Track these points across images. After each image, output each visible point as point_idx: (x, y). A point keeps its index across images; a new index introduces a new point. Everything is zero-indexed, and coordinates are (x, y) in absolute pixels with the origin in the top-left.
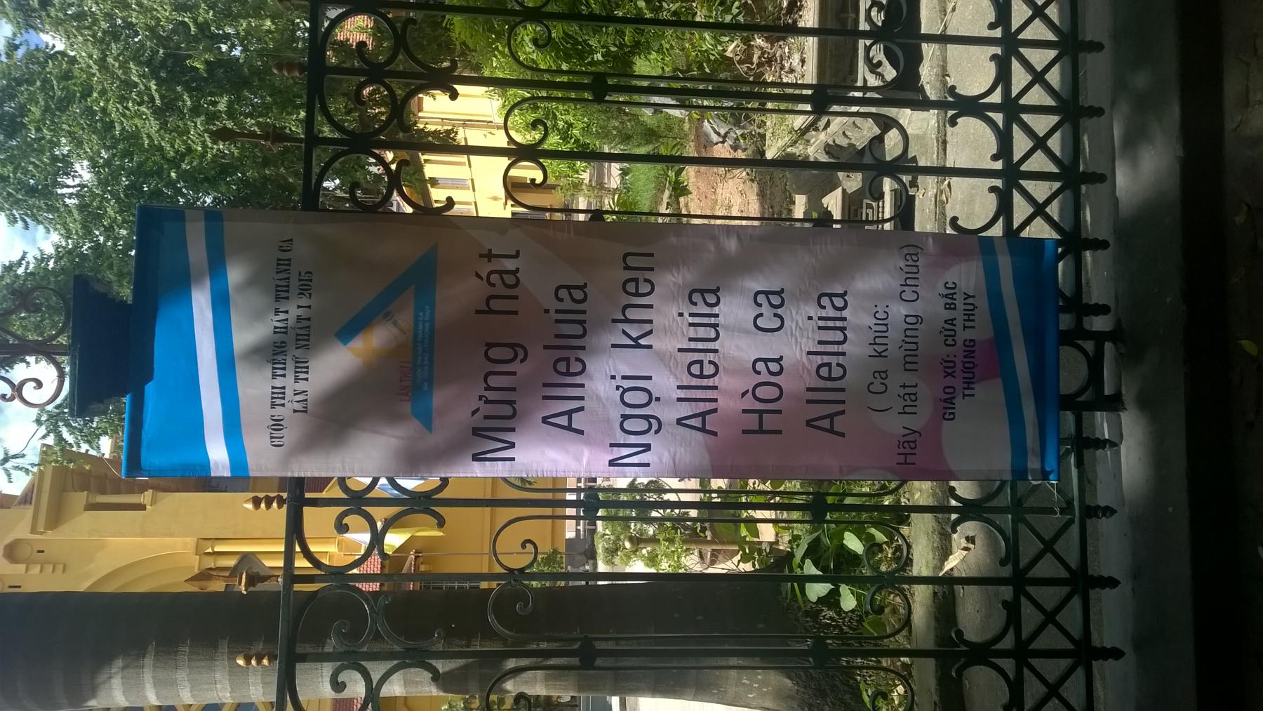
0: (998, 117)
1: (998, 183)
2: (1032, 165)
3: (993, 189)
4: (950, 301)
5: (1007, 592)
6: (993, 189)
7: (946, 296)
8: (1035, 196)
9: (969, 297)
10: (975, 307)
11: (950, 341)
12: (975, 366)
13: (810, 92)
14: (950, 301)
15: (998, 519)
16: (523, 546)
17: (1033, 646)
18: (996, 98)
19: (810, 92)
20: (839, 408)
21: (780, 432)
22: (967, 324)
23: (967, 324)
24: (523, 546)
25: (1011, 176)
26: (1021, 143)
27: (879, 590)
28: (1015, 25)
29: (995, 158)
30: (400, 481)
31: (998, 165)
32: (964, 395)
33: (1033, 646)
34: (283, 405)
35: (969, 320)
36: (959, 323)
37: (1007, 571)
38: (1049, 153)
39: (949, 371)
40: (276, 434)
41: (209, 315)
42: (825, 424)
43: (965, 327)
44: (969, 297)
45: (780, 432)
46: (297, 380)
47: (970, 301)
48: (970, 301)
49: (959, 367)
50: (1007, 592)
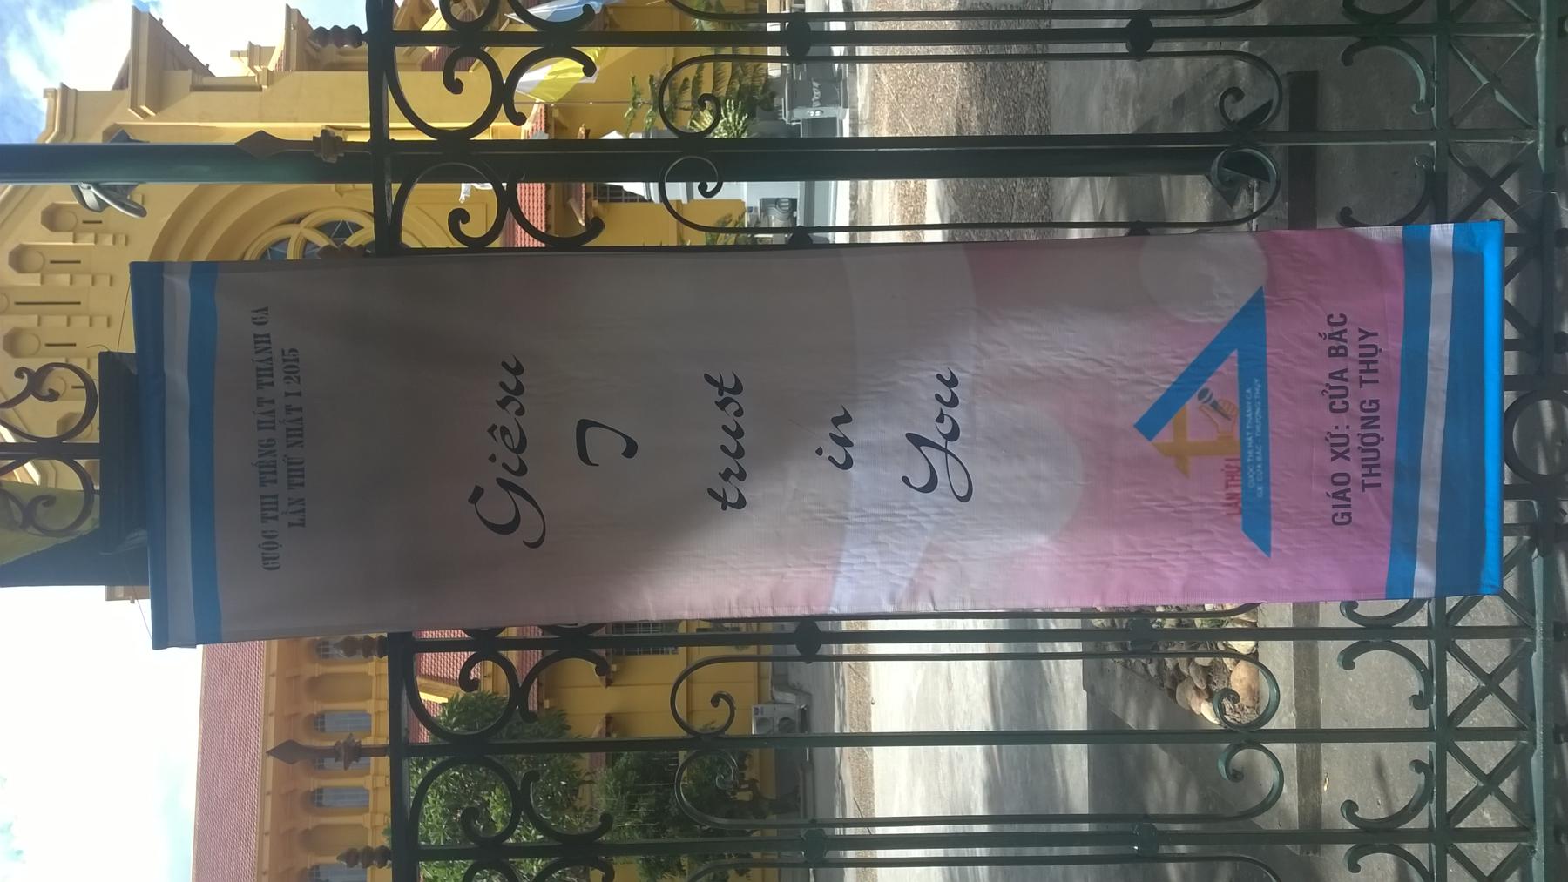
0: (1420, 648)
2: (1476, 719)
4: (1334, 343)
5: (1424, 750)
6: (1418, 765)
7: (1331, 336)
8: (1481, 866)
9: (1368, 334)
10: (1378, 351)
11: (1339, 405)
13: (1124, 23)
14: (1334, 343)
15: (1411, 848)
19: (1124, 23)
22: (1365, 377)
26: (1460, 681)
27: (1238, 747)
28: (1454, 701)
30: (533, 11)
31: (1420, 719)
32: (1364, 486)
34: (275, 518)
35: (1368, 371)
36: (1353, 374)
37: (1420, 719)
38: (1502, 696)
39: (1340, 450)
40: (271, 554)
44: (1368, 334)
46: (291, 486)
47: (1368, 341)
48: (1368, 341)
49: (1355, 443)
50: (1424, 750)
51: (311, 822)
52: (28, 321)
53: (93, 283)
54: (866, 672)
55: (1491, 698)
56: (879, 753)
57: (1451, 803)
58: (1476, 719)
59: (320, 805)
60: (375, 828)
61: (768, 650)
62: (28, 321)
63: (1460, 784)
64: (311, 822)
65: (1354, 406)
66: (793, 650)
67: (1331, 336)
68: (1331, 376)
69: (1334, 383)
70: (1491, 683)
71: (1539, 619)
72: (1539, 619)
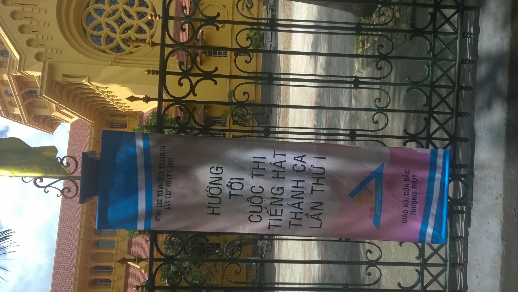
1: (418, 268)
3: (417, 271)
5: (426, 115)
12: (417, 203)
16: (48, 191)
17: (433, 137)
18: (430, 29)
20: (320, 212)
21: (208, 214)
23: (412, 213)
24: (48, 191)
25: (424, 264)
29: (418, 258)
31: (419, 261)
33: (433, 137)
41: (434, 196)
42: (297, 206)
43: (411, 214)
44: (415, 176)
45: (208, 214)
50: (426, 115)
51: (96, 251)
52: (19, 8)
53: (42, 38)
54: (289, 90)
55: (436, 255)
56: (293, 57)
57: (426, 257)
58: (437, 135)
59: (98, 246)
60: (117, 254)
61: (255, 134)
62: (19, 8)
63: (427, 278)
64: (96, 251)
65: (410, 194)
66: (263, 135)
67: (405, 176)
68: (405, 185)
69: (405, 187)
70: (435, 278)
71: (448, 263)
72: (448, 263)
